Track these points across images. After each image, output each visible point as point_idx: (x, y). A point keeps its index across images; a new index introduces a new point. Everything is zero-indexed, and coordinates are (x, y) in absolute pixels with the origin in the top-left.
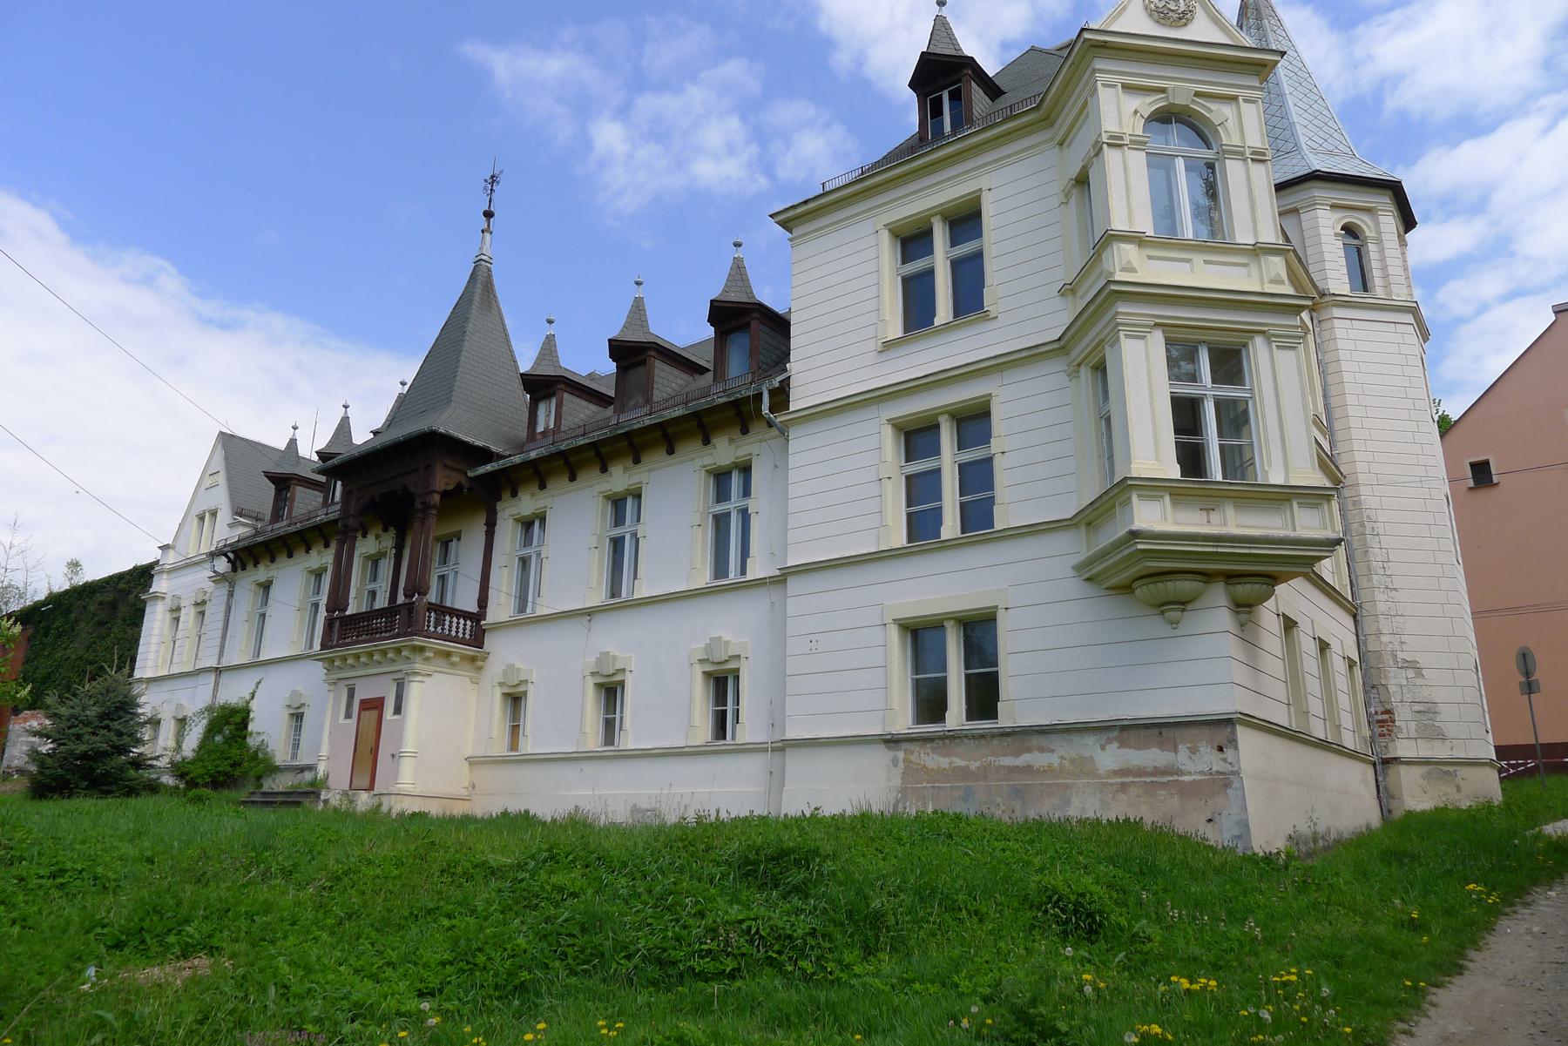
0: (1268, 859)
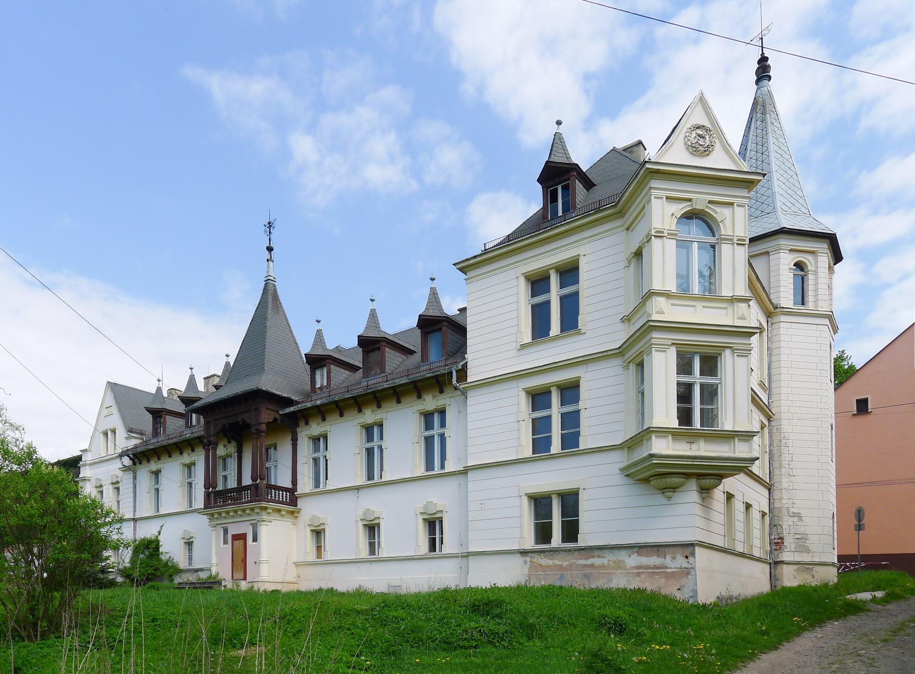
0: (704, 606)
